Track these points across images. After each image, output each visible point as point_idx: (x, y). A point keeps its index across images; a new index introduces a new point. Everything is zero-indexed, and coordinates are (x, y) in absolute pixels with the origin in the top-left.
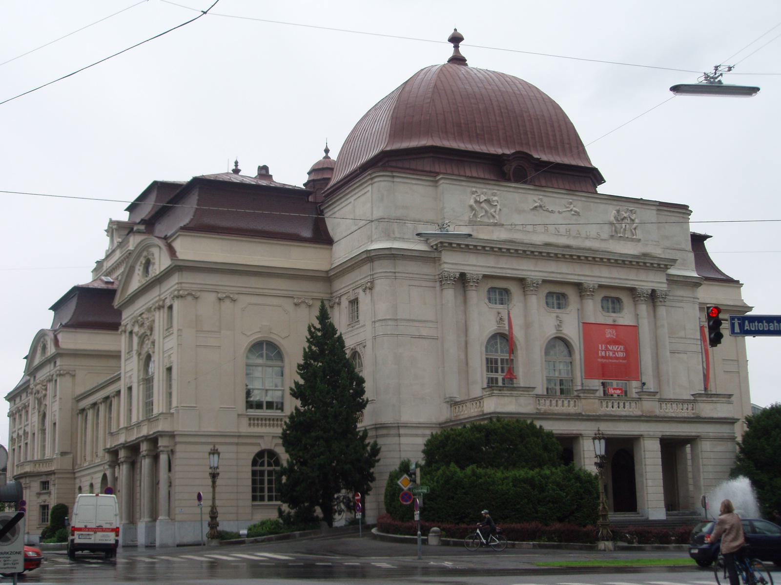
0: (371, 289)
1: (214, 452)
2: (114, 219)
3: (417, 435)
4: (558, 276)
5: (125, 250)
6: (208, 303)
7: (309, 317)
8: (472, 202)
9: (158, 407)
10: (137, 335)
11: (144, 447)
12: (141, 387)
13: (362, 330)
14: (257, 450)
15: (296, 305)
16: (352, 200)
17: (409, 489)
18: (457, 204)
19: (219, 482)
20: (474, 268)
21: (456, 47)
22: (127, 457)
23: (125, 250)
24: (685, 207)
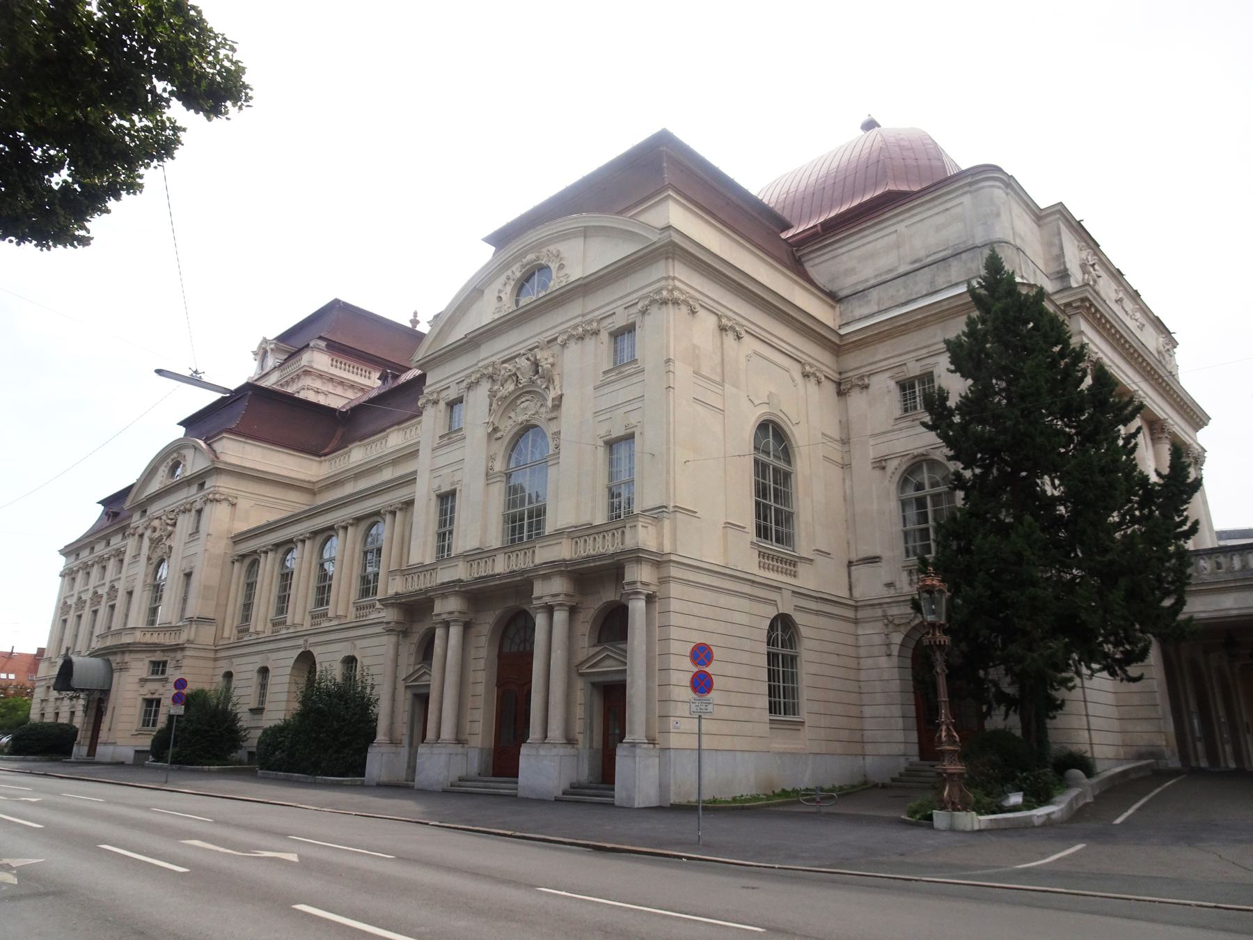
9: (163, 615)
16: (901, 227)
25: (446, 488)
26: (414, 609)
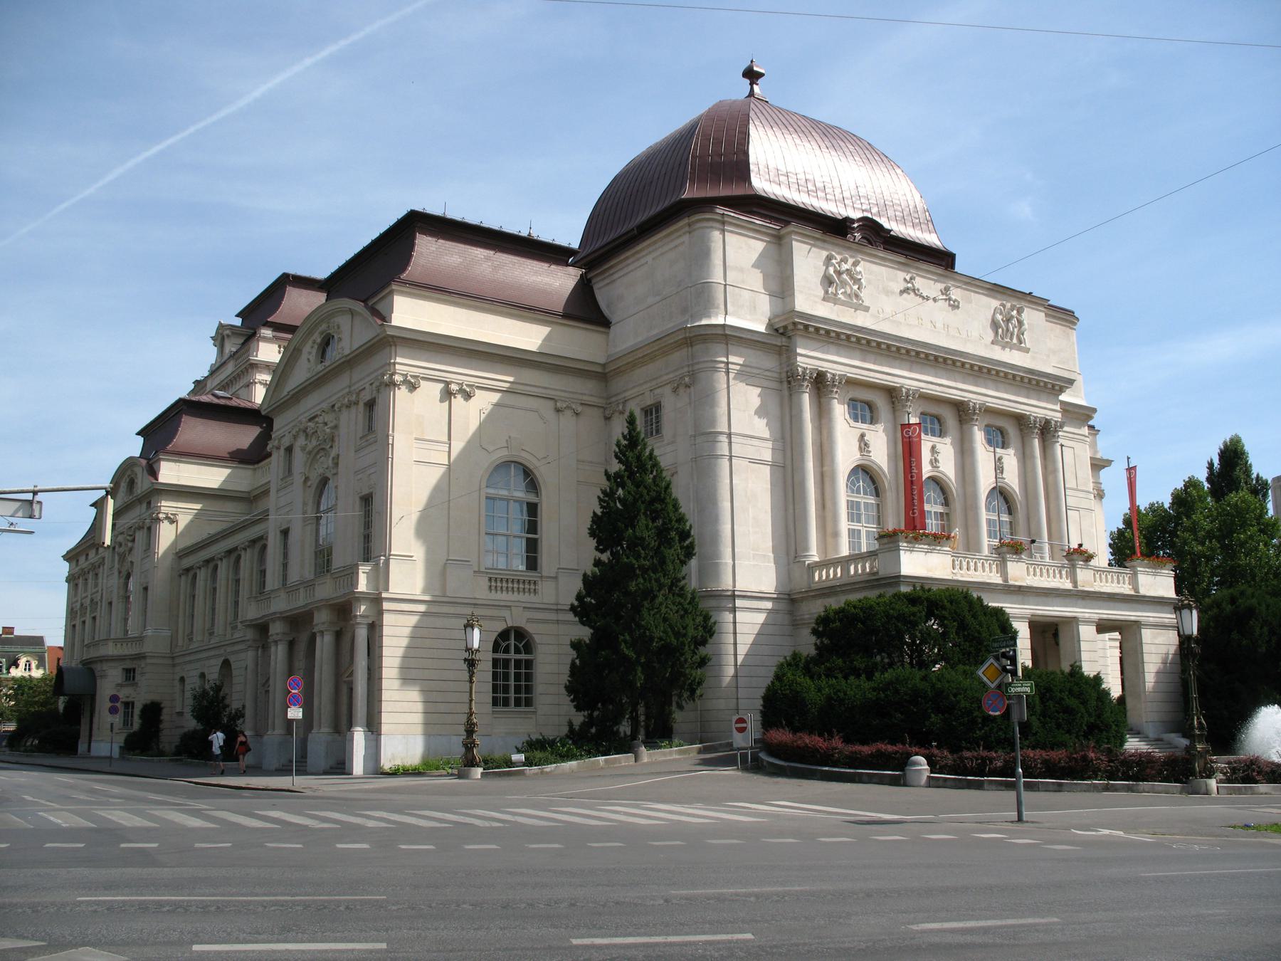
14: (501, 627)
15: (558, 410)
16: (649, 258)
20: (835, 366)
25: (365, 492)
26: (262, 628)
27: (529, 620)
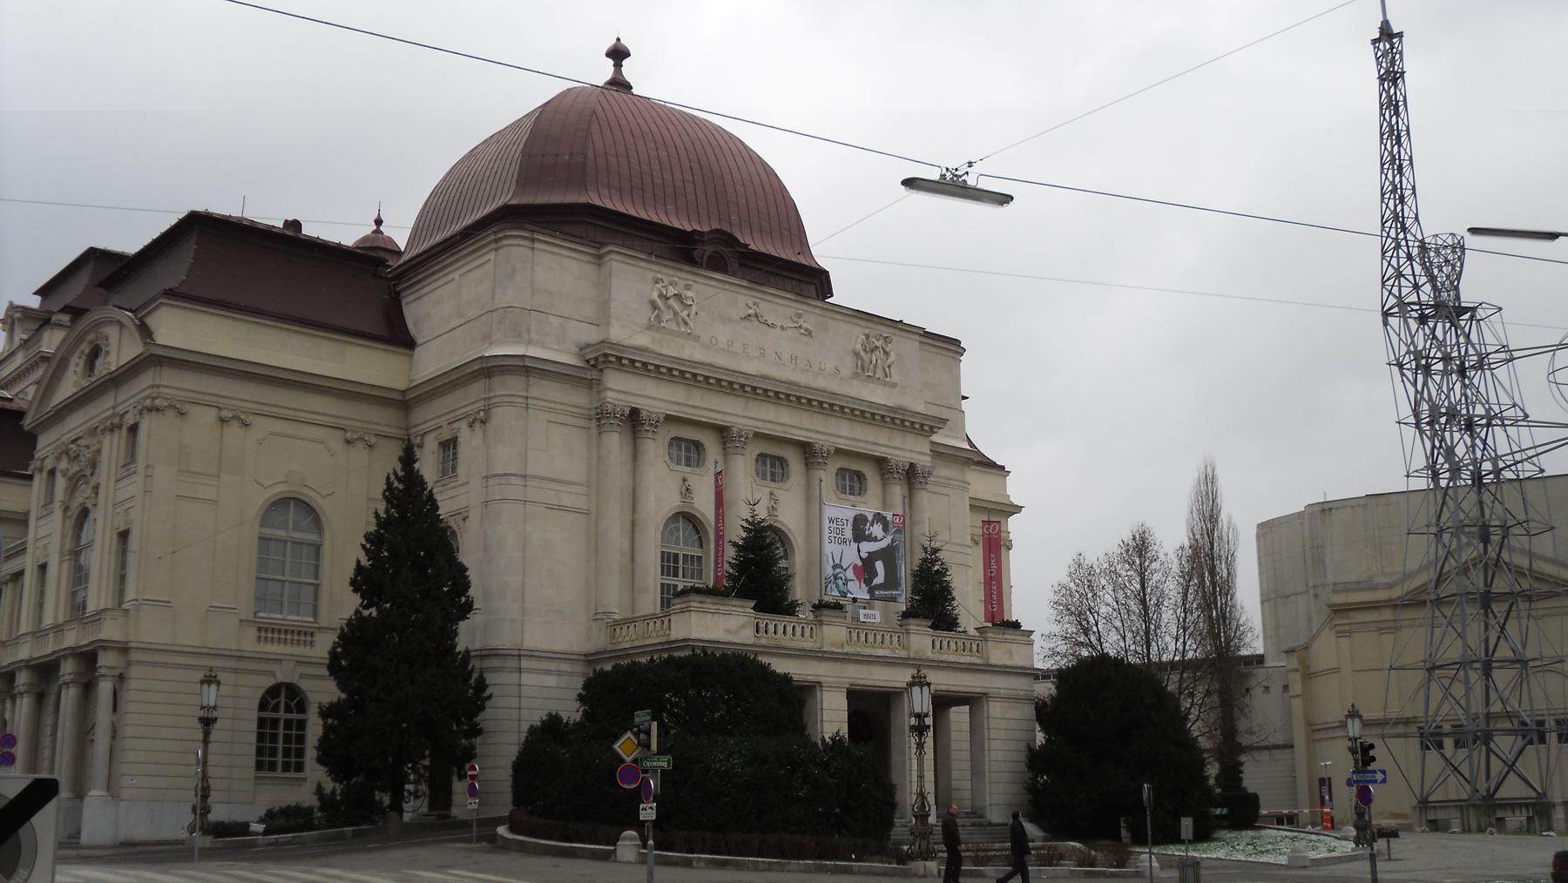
0: (483, 422)
1: (210, 680)
2: (18, 302)
3: (548, 672)
4: (778, 428)
5: (32, 352)
6: (200, 426)
7: (387, 461)
8: (655, 296)
9: (98, 596)
10: (64, 475)
11: (68, 668)
12: (66, 565)
13: (462, 490)
14: (269, 682)
15: (348, 442)
16: (456, 275)
17: (635, 761)
18: (631, 298)
19: (215, 735)
20: (653, 403)
21: (618, 66)
22: (31, 685)
23: (32, 352)
24: (956, 342)
27: (302, 676)
